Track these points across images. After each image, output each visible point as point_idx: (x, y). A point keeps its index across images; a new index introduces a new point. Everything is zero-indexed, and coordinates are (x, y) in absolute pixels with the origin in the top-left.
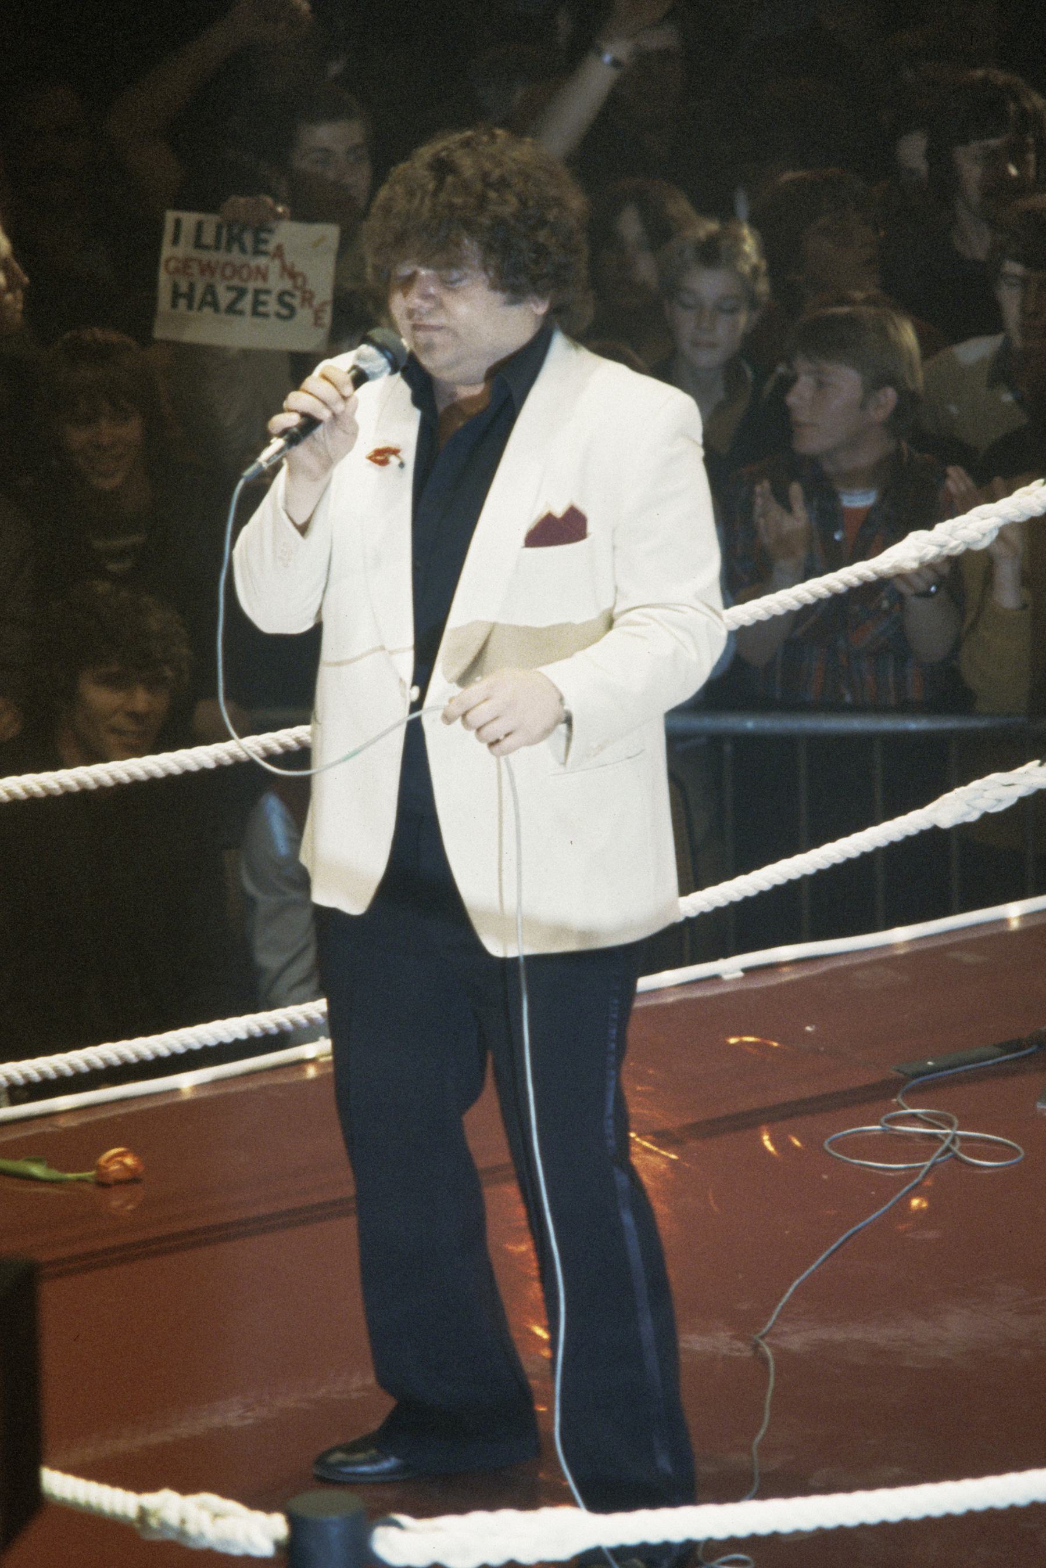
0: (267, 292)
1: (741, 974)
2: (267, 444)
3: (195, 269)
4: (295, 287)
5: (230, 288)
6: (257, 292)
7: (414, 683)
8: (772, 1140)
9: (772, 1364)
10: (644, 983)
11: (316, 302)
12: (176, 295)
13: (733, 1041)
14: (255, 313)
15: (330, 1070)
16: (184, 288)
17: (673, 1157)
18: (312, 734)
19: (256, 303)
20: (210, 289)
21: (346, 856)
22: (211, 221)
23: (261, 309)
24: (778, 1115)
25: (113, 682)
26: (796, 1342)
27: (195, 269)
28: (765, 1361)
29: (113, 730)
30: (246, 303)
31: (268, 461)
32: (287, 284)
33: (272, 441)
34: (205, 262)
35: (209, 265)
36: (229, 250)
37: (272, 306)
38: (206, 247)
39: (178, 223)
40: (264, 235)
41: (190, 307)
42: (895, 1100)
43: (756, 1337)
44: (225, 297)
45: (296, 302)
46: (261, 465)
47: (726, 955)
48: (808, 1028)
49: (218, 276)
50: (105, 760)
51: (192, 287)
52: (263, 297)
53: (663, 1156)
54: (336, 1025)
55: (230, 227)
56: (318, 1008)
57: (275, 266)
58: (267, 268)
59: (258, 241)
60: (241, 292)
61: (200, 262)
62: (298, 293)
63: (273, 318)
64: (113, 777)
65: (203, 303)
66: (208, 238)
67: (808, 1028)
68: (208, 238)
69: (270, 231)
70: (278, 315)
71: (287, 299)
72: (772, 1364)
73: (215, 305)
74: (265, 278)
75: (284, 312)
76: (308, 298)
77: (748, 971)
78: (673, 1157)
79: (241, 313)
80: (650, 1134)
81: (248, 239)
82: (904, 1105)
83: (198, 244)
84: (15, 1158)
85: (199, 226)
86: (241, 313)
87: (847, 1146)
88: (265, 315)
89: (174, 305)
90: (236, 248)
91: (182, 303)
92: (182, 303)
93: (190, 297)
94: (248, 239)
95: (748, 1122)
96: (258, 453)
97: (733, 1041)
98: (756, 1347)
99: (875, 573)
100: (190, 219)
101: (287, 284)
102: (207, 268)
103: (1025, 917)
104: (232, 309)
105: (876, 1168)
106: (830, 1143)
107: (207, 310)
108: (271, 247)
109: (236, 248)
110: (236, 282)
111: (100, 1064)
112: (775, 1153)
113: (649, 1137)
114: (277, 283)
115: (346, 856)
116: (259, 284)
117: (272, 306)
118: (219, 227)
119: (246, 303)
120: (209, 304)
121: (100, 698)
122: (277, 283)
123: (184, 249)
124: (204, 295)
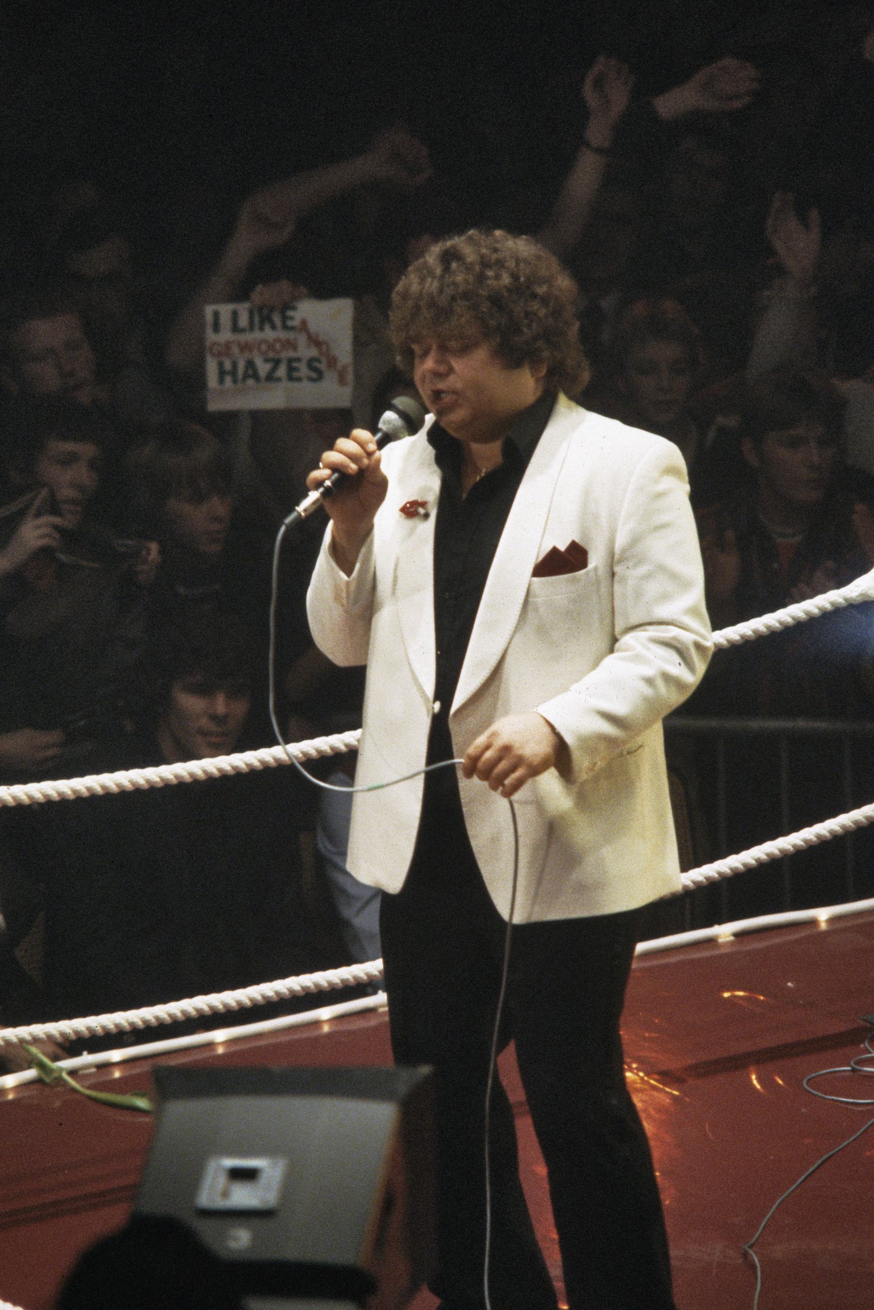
0: (298, 360)
1: (732, 938)
2: (305, 495)
3: (235, 350)
4: (321, 354)
5: (267, 360)
6: (290, 361)
7: (437, 697)
8: (759, 1079)
9: (759, 1269)
10: (641, 947)
11: (339, 365)
12: (222, 373)
13: (726, 995)
14: (291, 378)
15: (387, 1018)
16: (228, 366)
17: (676, 1093)
18: (363, 734)
19: (291, 369)
20: (250, 364)
21: (380, 850)
22: (243, 309)
23: (295, 374)
24: (762, 1058)
25: (204, 690)
26: (779, 1251)
27: (235, 350)
28: (753, 1267)
29: (202, 732)
30: (282, 371)
31: (305, 510)
32: (313, 352)
33: (310, 493)
34: (243, 343)
35: (246, 343)
36: (261, 329)
37: (304, 370)
38: (243, 331)
39: (216, 314)
40: (290, 313)
41: (235, 381)
42: (862, 1046)
43: (746, 1247)
44: (263, 368)
45: (323, 366)
46: (300, 514)
47: (720, 922)
48: (789, 984)
49: (255, 351)
50: (199, 757)
51: (235, 365)
52: (295, 365)
53: (667, 1092)
54: (389, 981)
55: (260, 310)
56: (375, 967)
57: (302, 340)
58: (296, 339)
59: (284, 318)
60: (277, 362)
61: (239, 344)
62: (324, 360)
63: (305, 380)
64: (205, 772)
65: (246, 376)
66: (243, 321)
67: (789, 984)
68: (243, 321)
69: (294, 308)
70: (311, 380)
71: (316, 364)
72: (759, 1269)
73: (256, 376)
74: (295, 347)
75: (314, 375)
76: (332, 362)
77: (740, 935)
78: (676, 1093)
79: (279, 380)
80: (656, 1073)
81: (277, 319)
82: (871, 1050)
83: (235, 329)
84: (123, 1092)
85: (235, 315)
86: (279, 380)
87: (835, 1084)
88: (299, 379)
89: (221, 380)
90: (267, 327)
91: (228, 379)
92: (228, 379)
93: (234, 372)
94: (277, 319)
95: (738, 1063)
96: (298, 504)
97: (726, 995)
98: (745, 1255)
99: (728, 641)
100: (225, 310)
101: (313, 352)
102: (245, 347)
103: (832, 920)
104: (270, 377)
105: (847, 1103)
106: (808, 1082)
107: (251, 382)
108: (296, 323)
109: (267, 327)
110: (271, 355)
111: (248, 1003)
112: (762, 1090)
113: (656, 1076)
114: (306, 352)
115: (380, 850)
116: (291, 354)
117: (304, 370)
118: (251, 312)
119: (282, 371)
120: (250, 376)
121: (191, 703)
122: (306, 352)
123: (225, 335)
124: (247, 368)
